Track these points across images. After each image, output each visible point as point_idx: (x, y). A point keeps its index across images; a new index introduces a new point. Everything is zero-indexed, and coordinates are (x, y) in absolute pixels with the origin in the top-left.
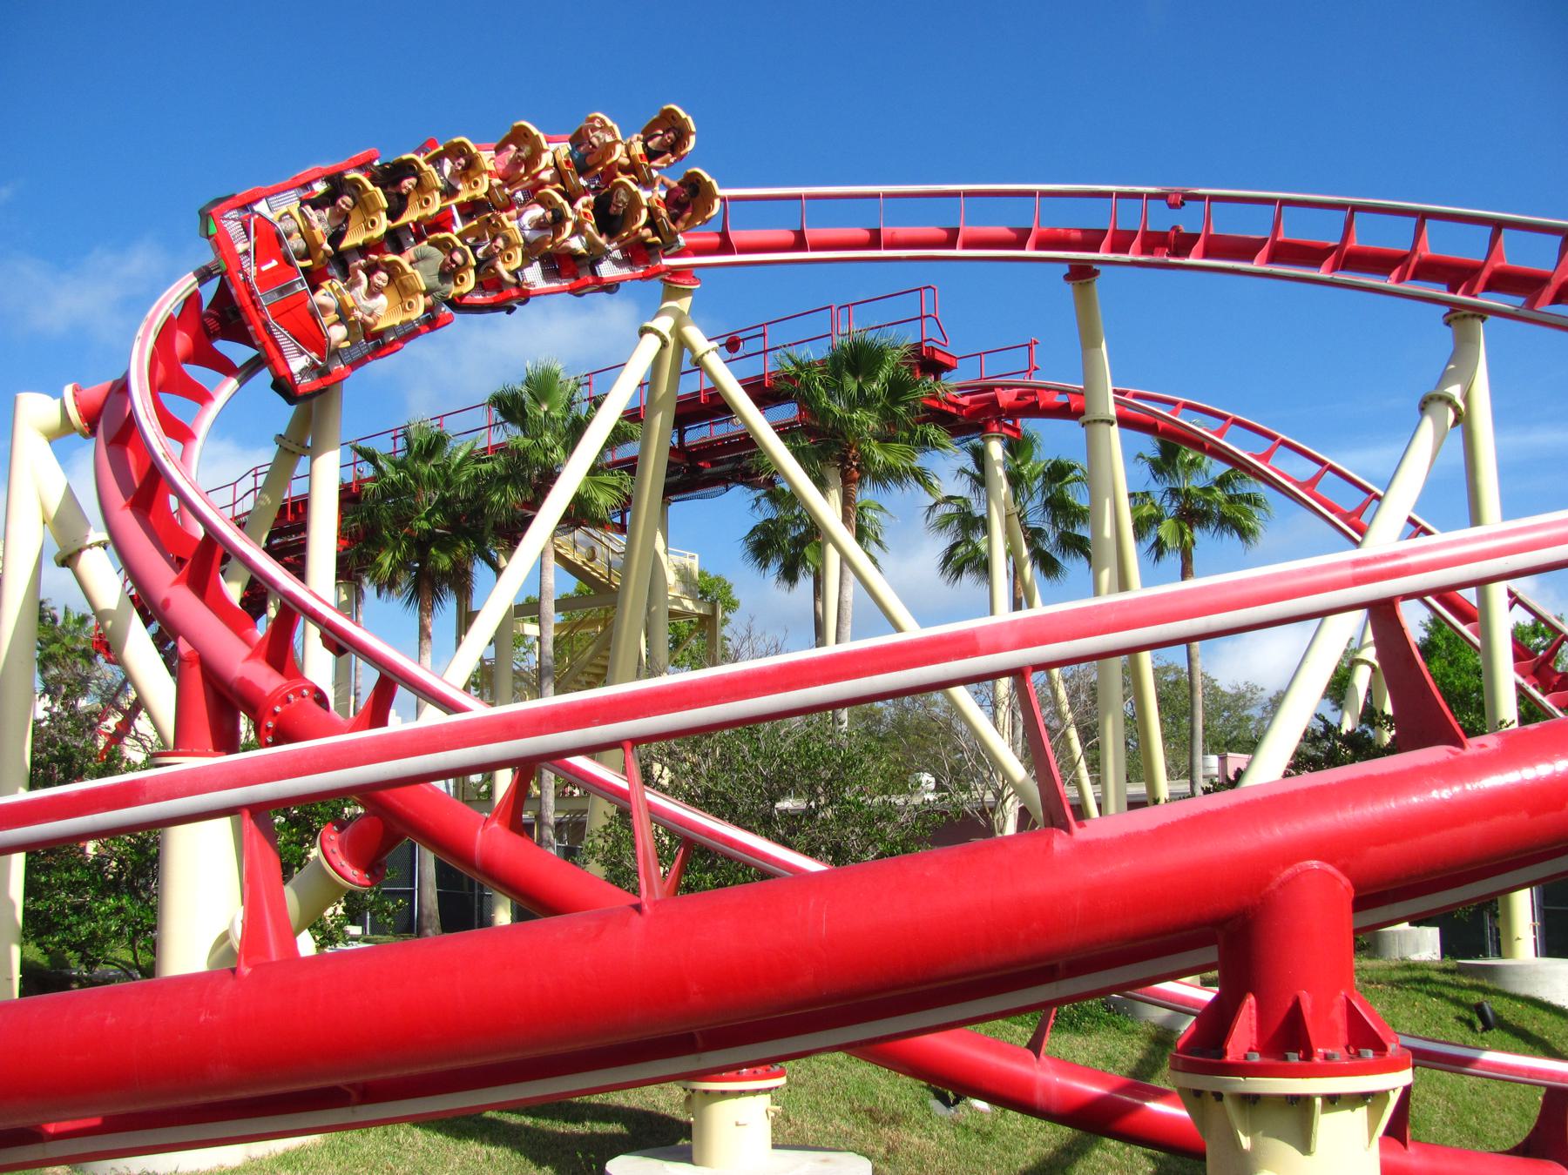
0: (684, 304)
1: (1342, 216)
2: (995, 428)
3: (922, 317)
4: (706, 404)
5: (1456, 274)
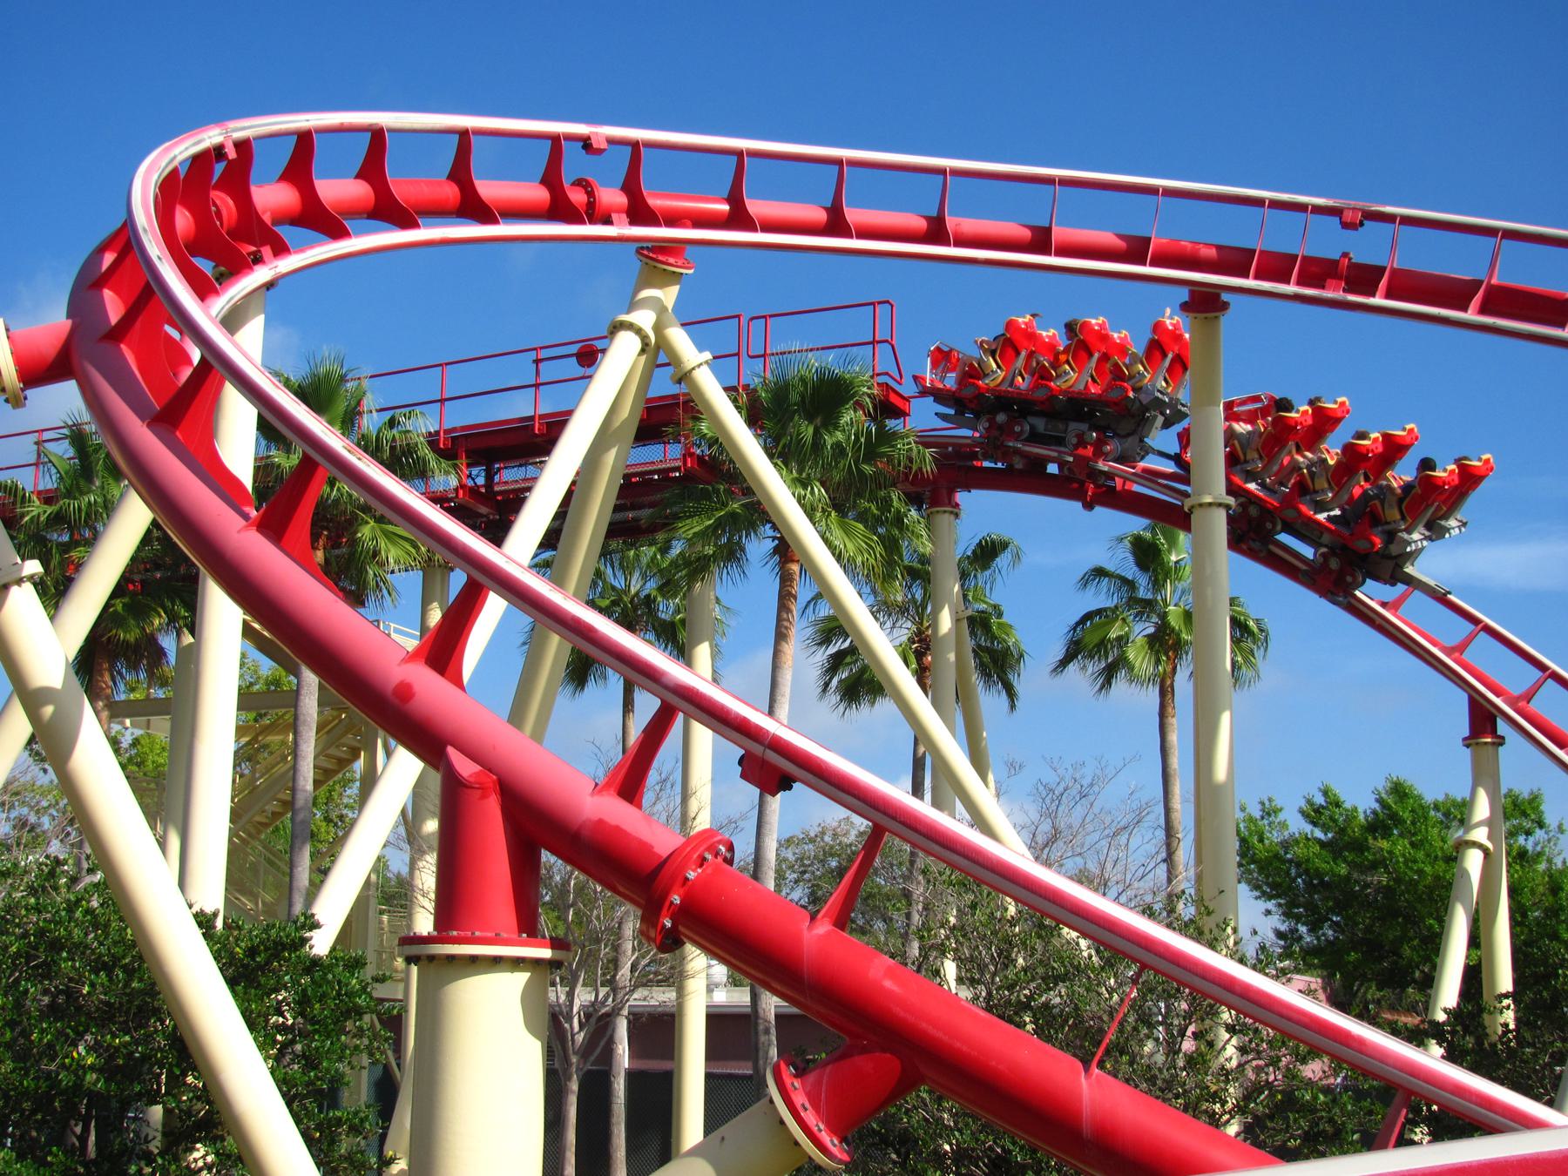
0: (669, 295)
3: (874, 343)
4: (542, 435)
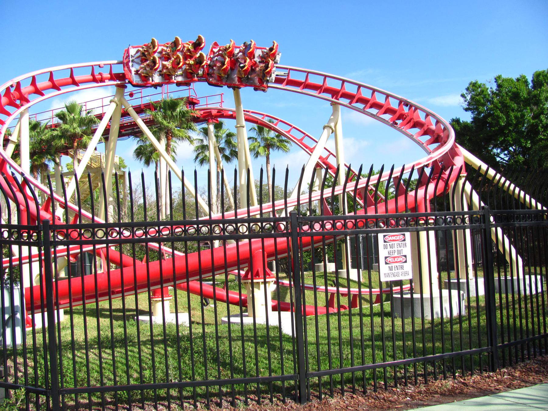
1: (306, 74)
2: (211, 121)
5: (334, 93)
